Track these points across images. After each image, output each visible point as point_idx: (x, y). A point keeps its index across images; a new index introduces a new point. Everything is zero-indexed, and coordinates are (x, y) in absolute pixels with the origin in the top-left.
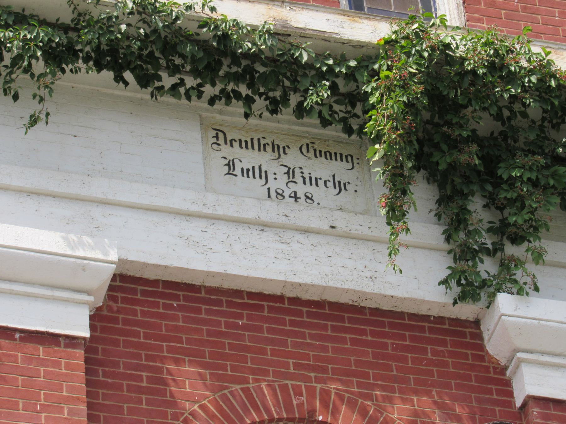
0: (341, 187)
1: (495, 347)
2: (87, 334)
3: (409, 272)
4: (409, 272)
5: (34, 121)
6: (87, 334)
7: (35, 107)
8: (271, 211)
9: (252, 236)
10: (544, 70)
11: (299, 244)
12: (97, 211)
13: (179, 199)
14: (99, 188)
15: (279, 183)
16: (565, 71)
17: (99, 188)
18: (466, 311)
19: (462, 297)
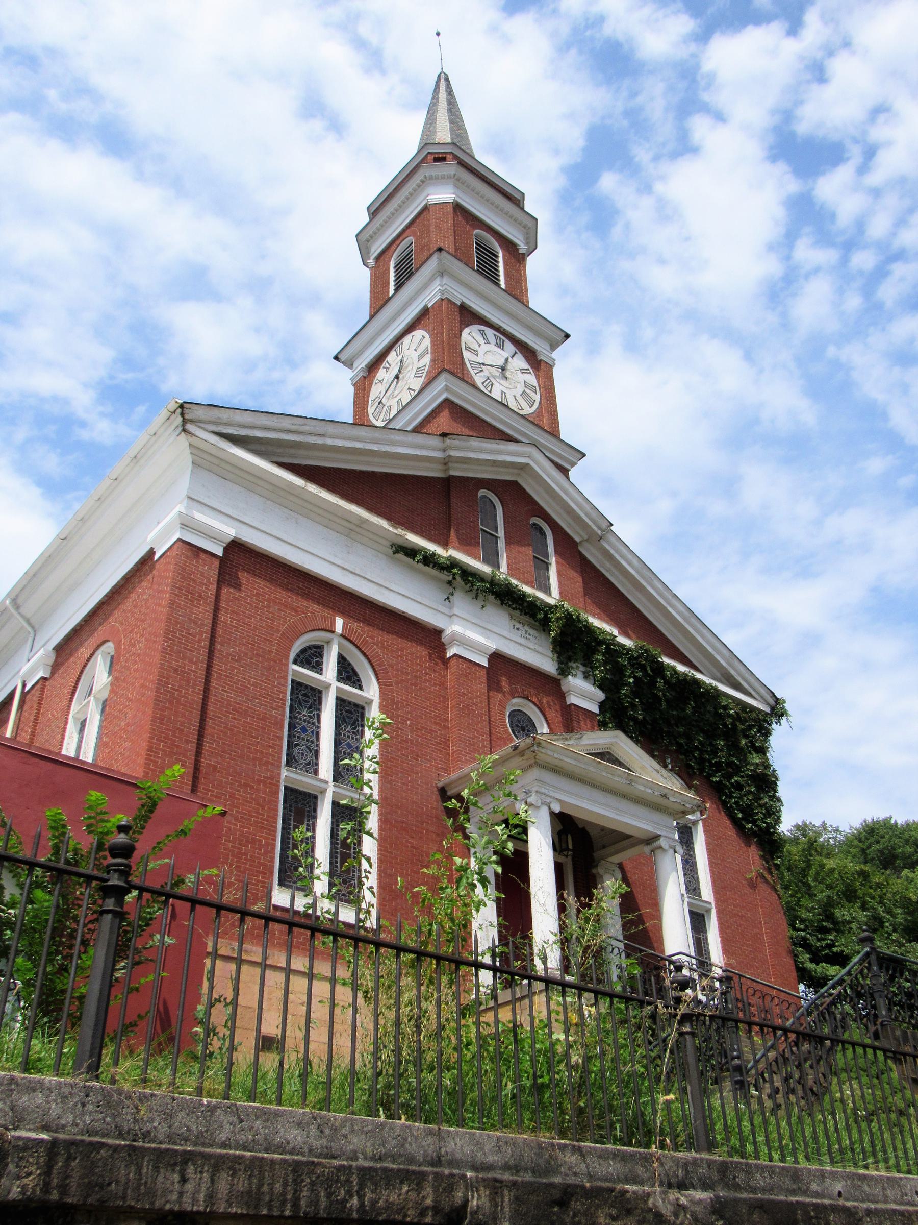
0: (536, 638)
1: (564, 688)
2: (221, 555)
3: (546, 663)
4: (546, 663)
5: (483, 607)
6: (221, 555)
7: (483, 603)
8: (523, 641)
9: (518, 647)
10: (586, 621)
11: (512, 645)
12: (488, 632)
13: (505, 633)
14: (489, 626)
15: (523, 634)
16: (884, 847)
17: (489, 626)
18: (559, 677)
19: (559, 674)
